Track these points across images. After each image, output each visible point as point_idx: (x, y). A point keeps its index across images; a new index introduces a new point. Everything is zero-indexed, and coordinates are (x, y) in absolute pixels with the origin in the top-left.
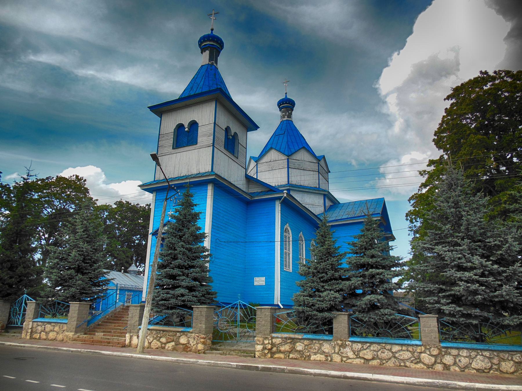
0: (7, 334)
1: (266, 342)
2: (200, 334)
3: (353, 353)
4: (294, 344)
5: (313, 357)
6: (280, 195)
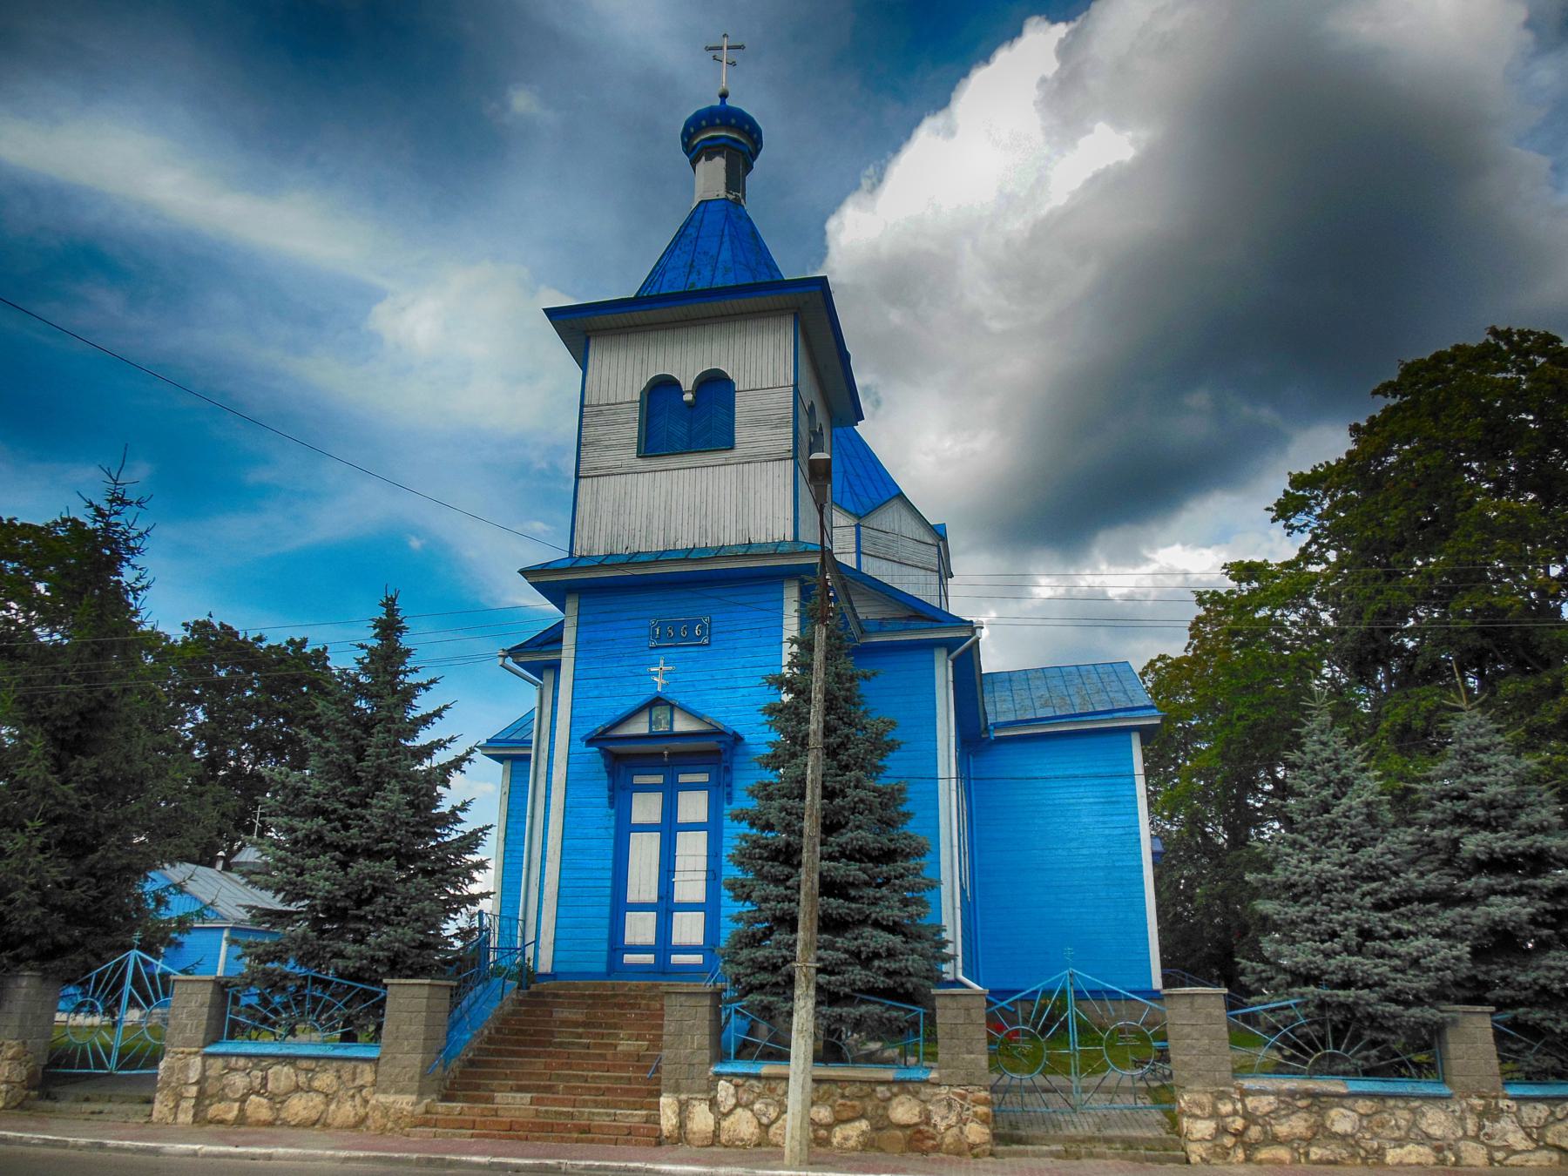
0: (48, 1104)
1: (1226, 1108)
2: (971, 1088)
3: (1524, 1136)
4: (1322, 1112)
5: (1392, 1155)
6: (958, 635)
